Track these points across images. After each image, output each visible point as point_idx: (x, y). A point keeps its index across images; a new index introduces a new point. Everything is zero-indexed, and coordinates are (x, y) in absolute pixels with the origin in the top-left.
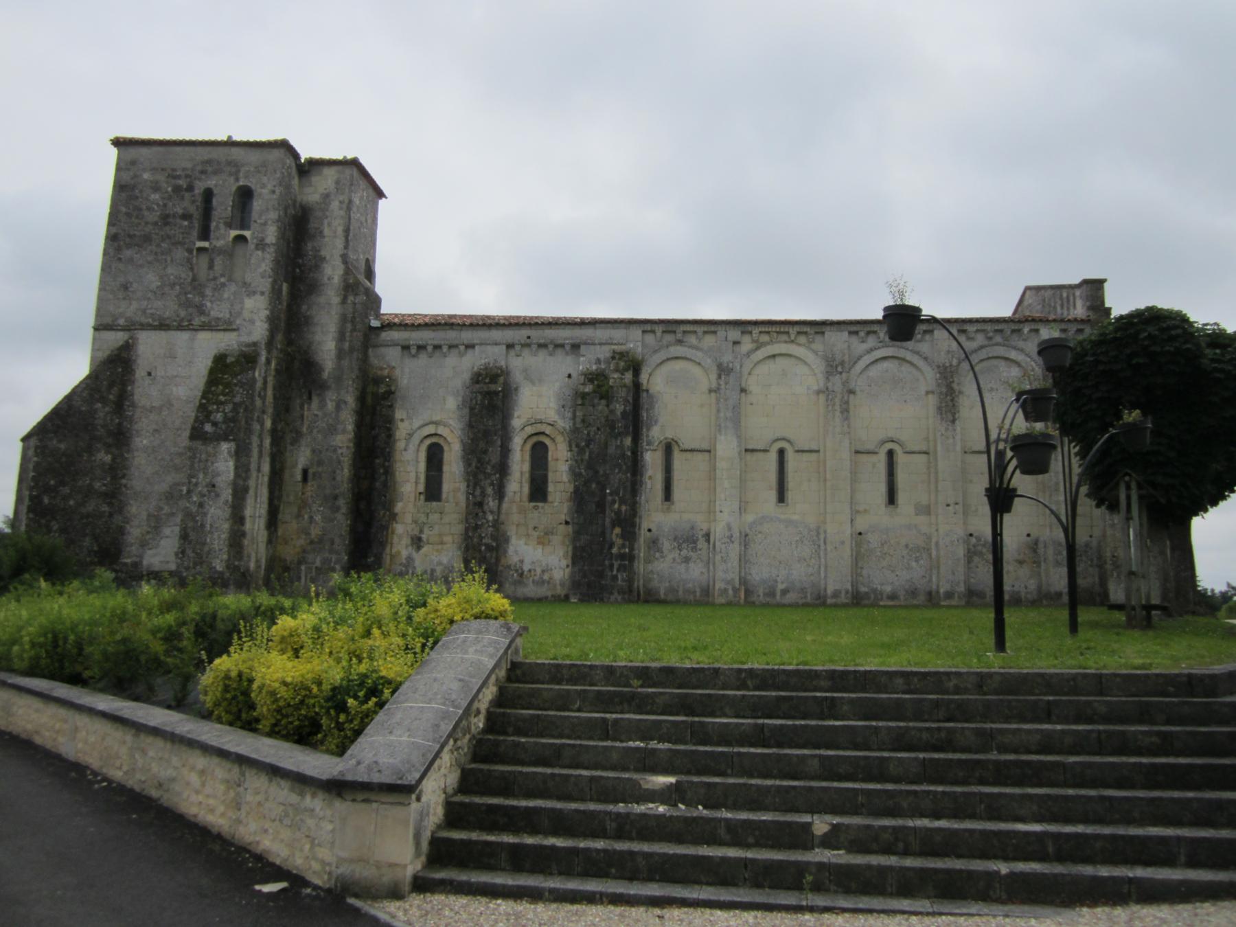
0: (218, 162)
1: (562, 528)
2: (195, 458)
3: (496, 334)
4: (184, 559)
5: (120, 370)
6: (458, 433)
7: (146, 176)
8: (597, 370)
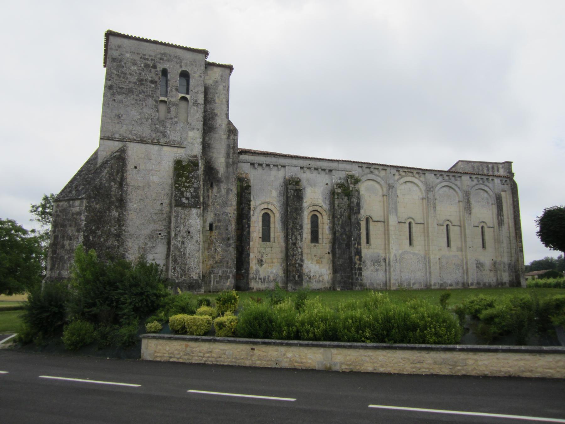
0: (169, 55)
1: (327, 256)
2: (178, 217)
3: (295, 162)
4: (176, 273)
5: (121, 164)
6: (278, 208)
7: (128, 55)
8: (340, 182)
